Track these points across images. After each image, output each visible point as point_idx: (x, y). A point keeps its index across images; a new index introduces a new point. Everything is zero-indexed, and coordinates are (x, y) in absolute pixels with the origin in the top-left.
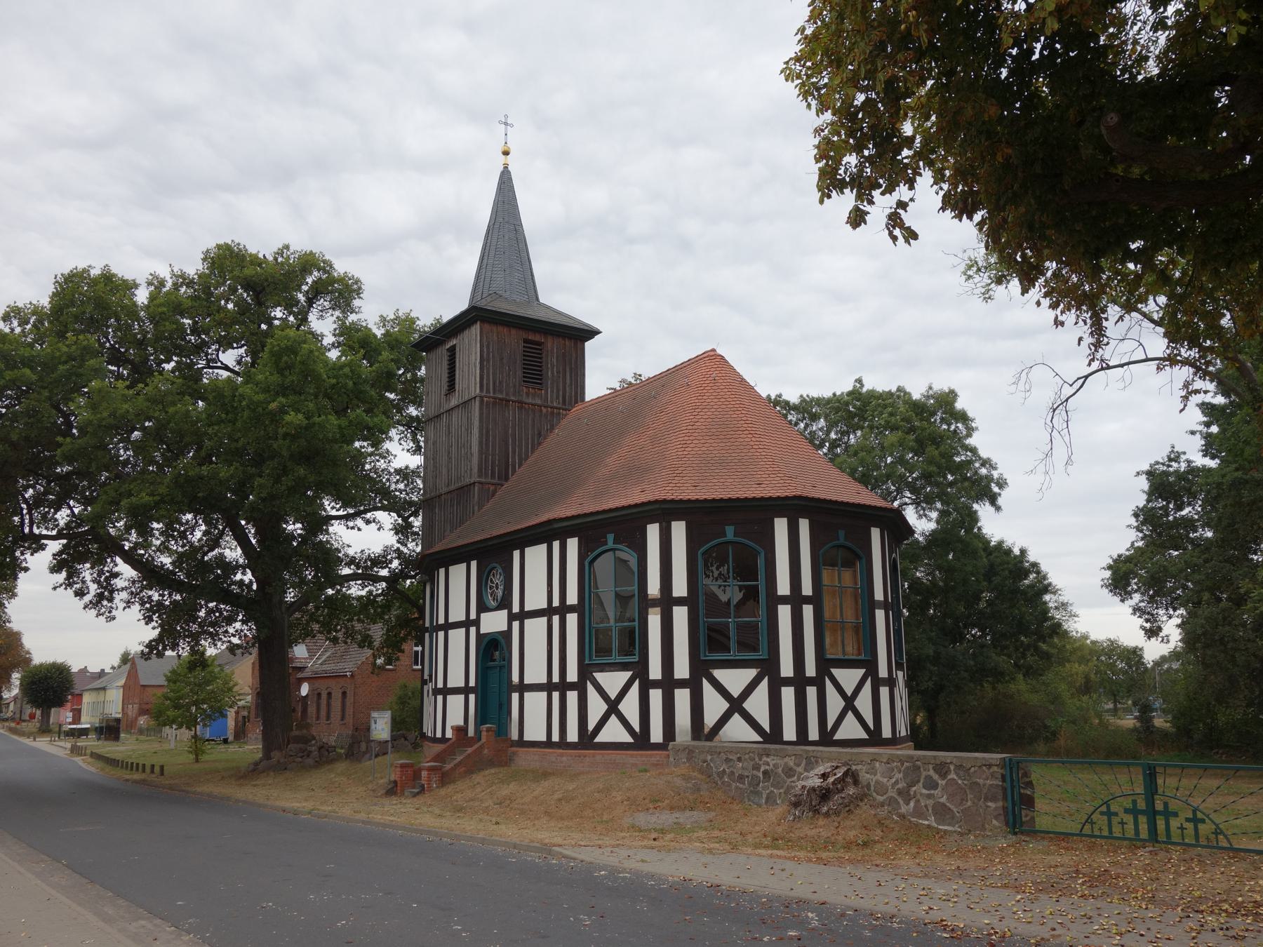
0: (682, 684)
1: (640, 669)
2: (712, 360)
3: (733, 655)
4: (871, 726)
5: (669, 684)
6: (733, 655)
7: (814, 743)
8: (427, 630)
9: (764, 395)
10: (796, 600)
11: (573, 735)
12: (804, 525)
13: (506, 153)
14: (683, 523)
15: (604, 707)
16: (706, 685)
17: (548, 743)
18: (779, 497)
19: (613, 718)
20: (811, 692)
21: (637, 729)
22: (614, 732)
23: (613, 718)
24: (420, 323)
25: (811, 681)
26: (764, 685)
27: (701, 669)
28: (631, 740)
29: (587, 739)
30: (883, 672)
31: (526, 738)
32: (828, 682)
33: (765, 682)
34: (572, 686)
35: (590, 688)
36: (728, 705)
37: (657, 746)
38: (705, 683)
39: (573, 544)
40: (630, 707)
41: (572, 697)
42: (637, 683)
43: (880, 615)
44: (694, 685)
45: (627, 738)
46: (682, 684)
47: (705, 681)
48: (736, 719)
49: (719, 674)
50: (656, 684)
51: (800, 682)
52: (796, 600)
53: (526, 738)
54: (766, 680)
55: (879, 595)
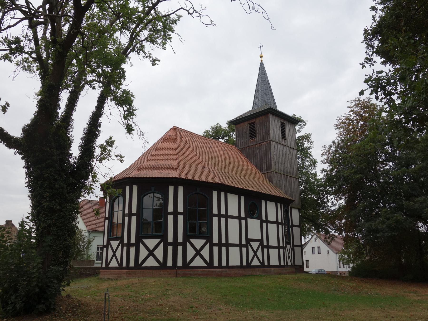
0: (180, 244)
1: (163, 238)
2: (175, 129)
3: (198, 234)
5: (129, 245)
6: (198, 234)
9: (201, 134)
10: (176, 213)
11: (132, 264)
12: (181, 190)
13: (261, 57)
14: (173, 186)
16: (141, 245)
17: (241, 266)
18: (131, 177)
20: (180, 249)
21: (208, 261)
24: (22, 156)
26: (162, 245)
27: (187, 238)
28: (206, 265)
31: (230, 264)
33: (162, 245)
34: (133, 245)
36: (154, 253)
37: (170, 268)
39: (135, 189)
40: (159, 253)
41: (133, 250)
45: (204, 264)
46: (180, 244)
47: (140, 244)
48: (198, 257)
49: (145, 241)
50: (170, 244)
51: (175, 244)
52: (176, 213)
53: (230, 264)
54: (162, 243)
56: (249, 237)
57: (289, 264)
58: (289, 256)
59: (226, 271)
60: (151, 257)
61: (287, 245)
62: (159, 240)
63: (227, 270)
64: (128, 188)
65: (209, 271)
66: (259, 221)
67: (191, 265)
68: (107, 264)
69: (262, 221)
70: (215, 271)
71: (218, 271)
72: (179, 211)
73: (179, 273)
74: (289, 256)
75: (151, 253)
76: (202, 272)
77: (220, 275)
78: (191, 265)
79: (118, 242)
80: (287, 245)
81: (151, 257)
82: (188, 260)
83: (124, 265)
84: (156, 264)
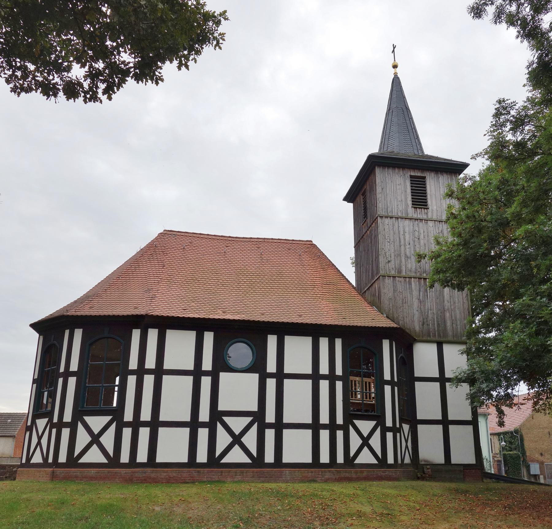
0: (204, 425)
1: (380, 419)
4: (380, 455)
7: (202, 465)
8: (363, 402)
11: (63, 458)
12: (338, 343)
15: (102, 439)
16: (80, 425)
19: (366, 449)
20: (340, 434)
22: (366, 457)
23: (366, 449)
25: (340, 427)
26: (255, 427)
27: (349, 418)
29: (349, 460)
30: (389, 423)
32: (351, 428)
33: (255, 426)
34: (67, 425)
35: (352, 430)
38: (219, 425)
39: (78, 334)
40: (108, 440)
42: (114, 424)
43: (388, 389)
44: (211, 426)
45: (374, 461)
46: (204, 425)
50: (128, 424)
51: (332, 427)
54: (256, 425)
55: (387, 376)
56: (221, 407)
57: (407, 460)
58: (407, 447)
59: (145, 473)
60: (237, 447)
61: (404, 425)
62: (109, 418)
63: (149, 470)
64: (67, 332)
65: (108, 472)
66: (255, 377)
67: (81, 461)
68: (29, 459)
69: (264, 377)
70: (121, 473)
71: (126, 473)
72: (285, 372)
73: (57, 475)
74: (407, 447)
75: (95, 439)
76: (96, 473)
77: (130, 481)
78: (81, 461)
79: (46, 420)
80: (404, 425)
81: (237, 447)
82: (77, 452)
83: (50, 460)
84: (246, 460)
